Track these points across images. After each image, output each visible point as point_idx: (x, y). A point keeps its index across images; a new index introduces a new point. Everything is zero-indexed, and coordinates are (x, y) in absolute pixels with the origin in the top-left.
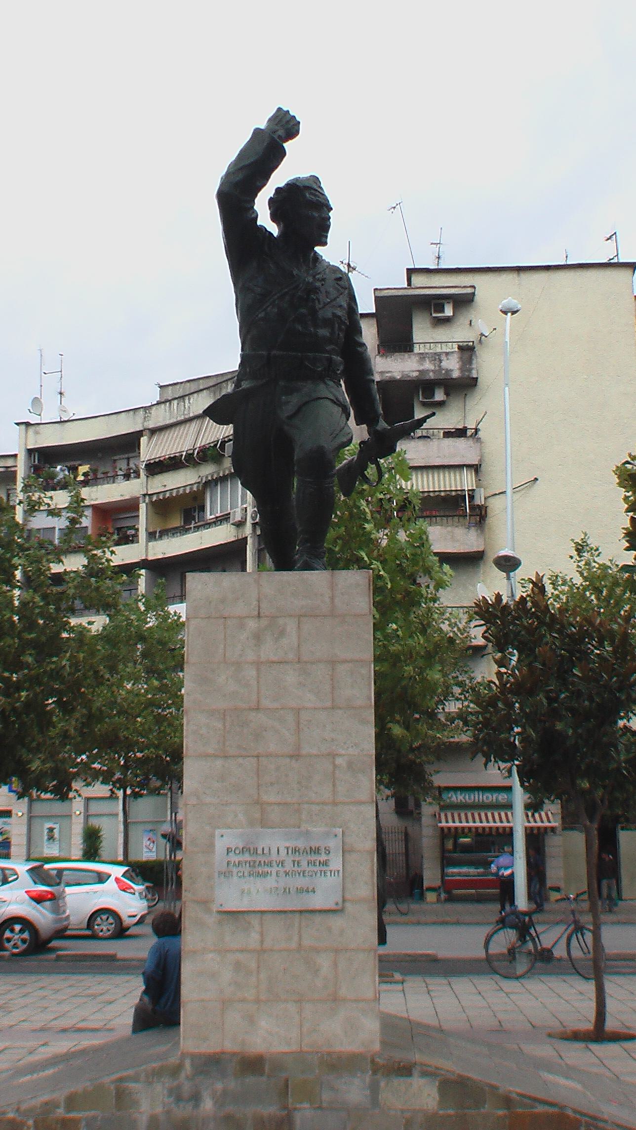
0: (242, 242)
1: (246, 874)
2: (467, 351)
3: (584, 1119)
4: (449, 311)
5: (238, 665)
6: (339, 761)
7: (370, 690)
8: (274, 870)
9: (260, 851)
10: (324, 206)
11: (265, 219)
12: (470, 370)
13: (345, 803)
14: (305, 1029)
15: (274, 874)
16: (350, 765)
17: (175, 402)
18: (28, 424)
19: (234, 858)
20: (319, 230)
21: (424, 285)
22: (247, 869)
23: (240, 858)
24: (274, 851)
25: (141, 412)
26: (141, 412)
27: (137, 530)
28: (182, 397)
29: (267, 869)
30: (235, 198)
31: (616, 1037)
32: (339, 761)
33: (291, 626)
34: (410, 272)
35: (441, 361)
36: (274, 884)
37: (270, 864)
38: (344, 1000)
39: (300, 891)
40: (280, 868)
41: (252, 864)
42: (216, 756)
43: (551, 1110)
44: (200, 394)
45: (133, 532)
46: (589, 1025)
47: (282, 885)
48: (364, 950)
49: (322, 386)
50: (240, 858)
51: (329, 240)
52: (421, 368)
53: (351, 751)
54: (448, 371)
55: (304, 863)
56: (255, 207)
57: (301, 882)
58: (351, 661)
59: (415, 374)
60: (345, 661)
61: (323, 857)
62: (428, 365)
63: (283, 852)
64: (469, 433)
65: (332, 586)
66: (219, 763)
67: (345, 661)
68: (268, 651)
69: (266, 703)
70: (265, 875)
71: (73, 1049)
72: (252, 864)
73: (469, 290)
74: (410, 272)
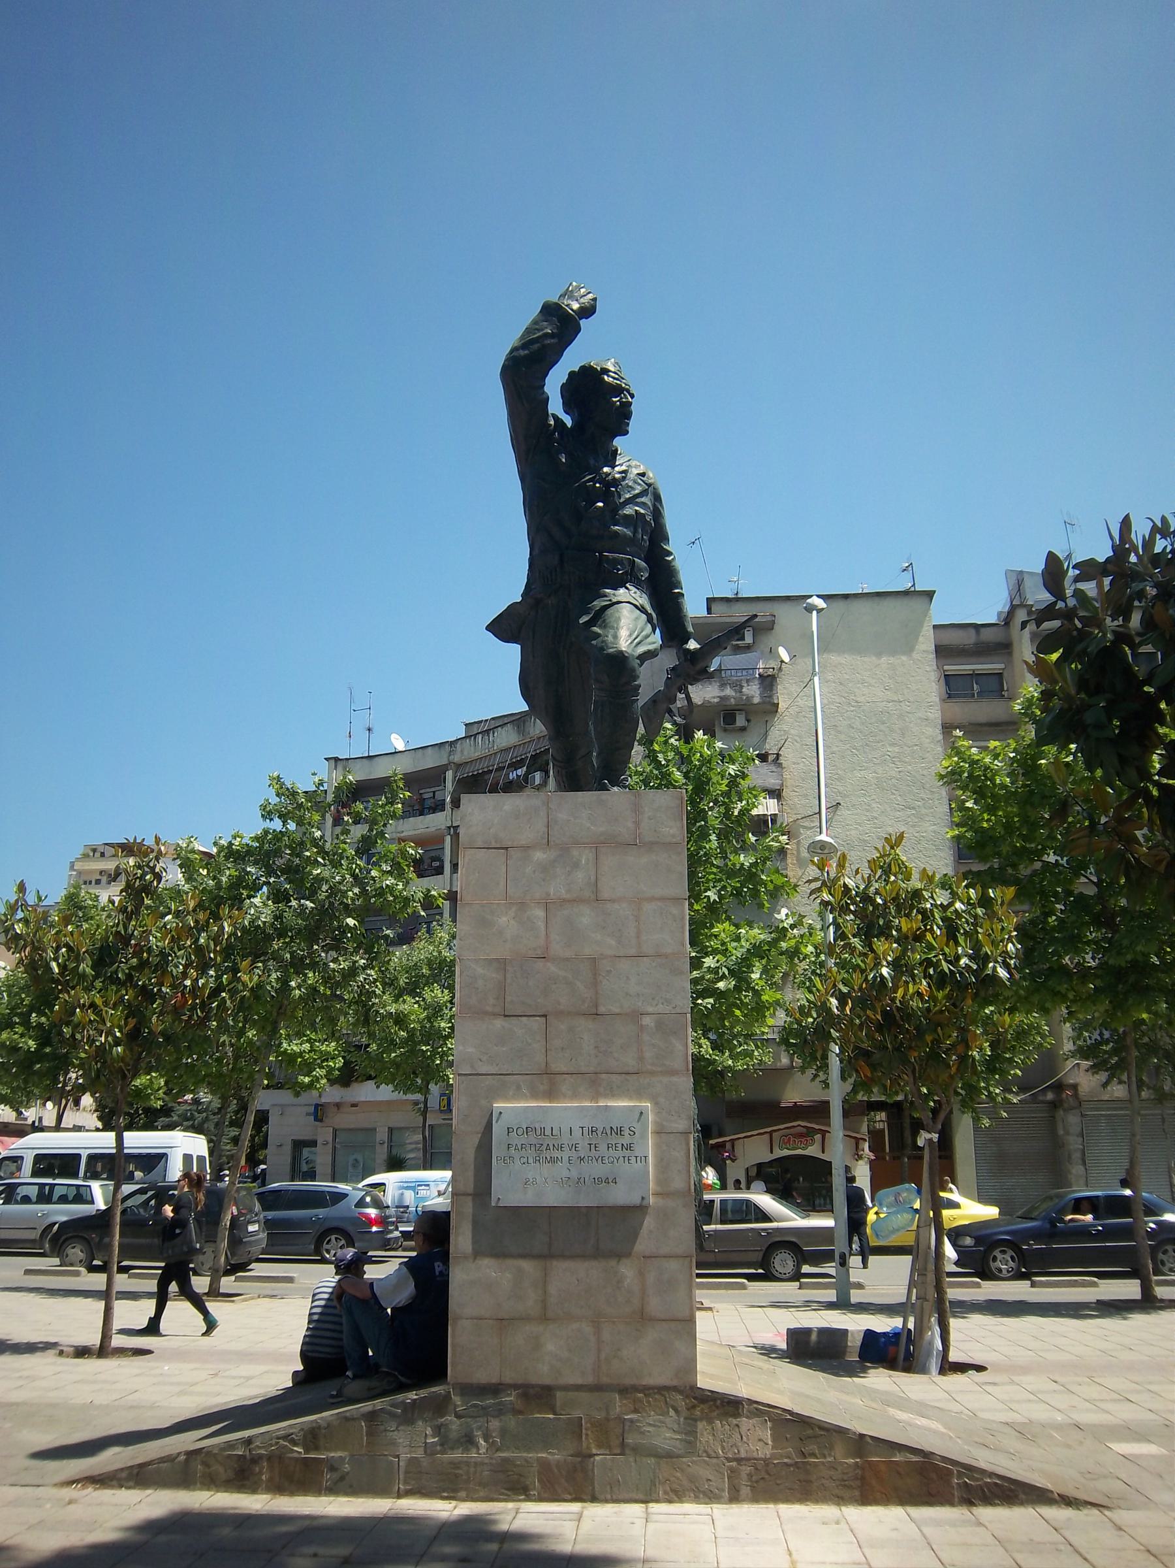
0: (533, 438)
1: (531, 1161)
2: (768, 681)
3: (954, 1469)
4: (749, 639)
5: (522, 906)
6: (647, 1021)
7: (683, 933)
8: (566, 1154)
9: (548, 1132)
10: (624, 412)
11: (556, 406)
12: (770, 697)
13: (652, 1073)
14: (603, 1356)
15: (565, 1159)
16: (660, 1025)
17: (480, 736)
18: (336, 759)
19: (516, 1140)
20: (620, 419)
21: (723, 614)
22: (531, 1153)
23: (524, 1139)
24: (565, 1130)
25: (447, 747)
26: (447, 747)
27: (442, 861)
28: (488, 731)
29: (557, 1154)
30: (523, 370)
31: (961, 1368)
32: (647, 1021)
33: (585, 857)
34: (710, 601)
35: (742, 687)
36: (565, 1173)
37: (561, 1148)
38: (653, 1319)
39: (598, 1181)
40: (573, 1153)
41: (538, 1148)
42: (495, 1015)
43: (915, 1459)
44: (505, 728)
45: (438, 864)
46: (94, 1339)
47: (574, 1174)
48: (677, 1257)
49: (622, 591)
50: (524, 1139)
51: (630, 429)
52: (722, 694)
53: (661, 1008)
54: (749, 698)
55: (603, 1147)
56: (546, 389)
57: (598, 1170)
58: (662, 899)
59: (716, 700)
60: (652, 899)
61: (626, 1140)
62: (729, 692)
63: (577, 1133)
64: (771, 758)
65: (637, 809)
66: (499, 1023)
67: (652, 899)
68: (557, 888)
69: (557, 949)
70: (553, 1160)
71: (116, 1403)
72: (538, 1148)
73: (769, 618)
74: (710, 601)
